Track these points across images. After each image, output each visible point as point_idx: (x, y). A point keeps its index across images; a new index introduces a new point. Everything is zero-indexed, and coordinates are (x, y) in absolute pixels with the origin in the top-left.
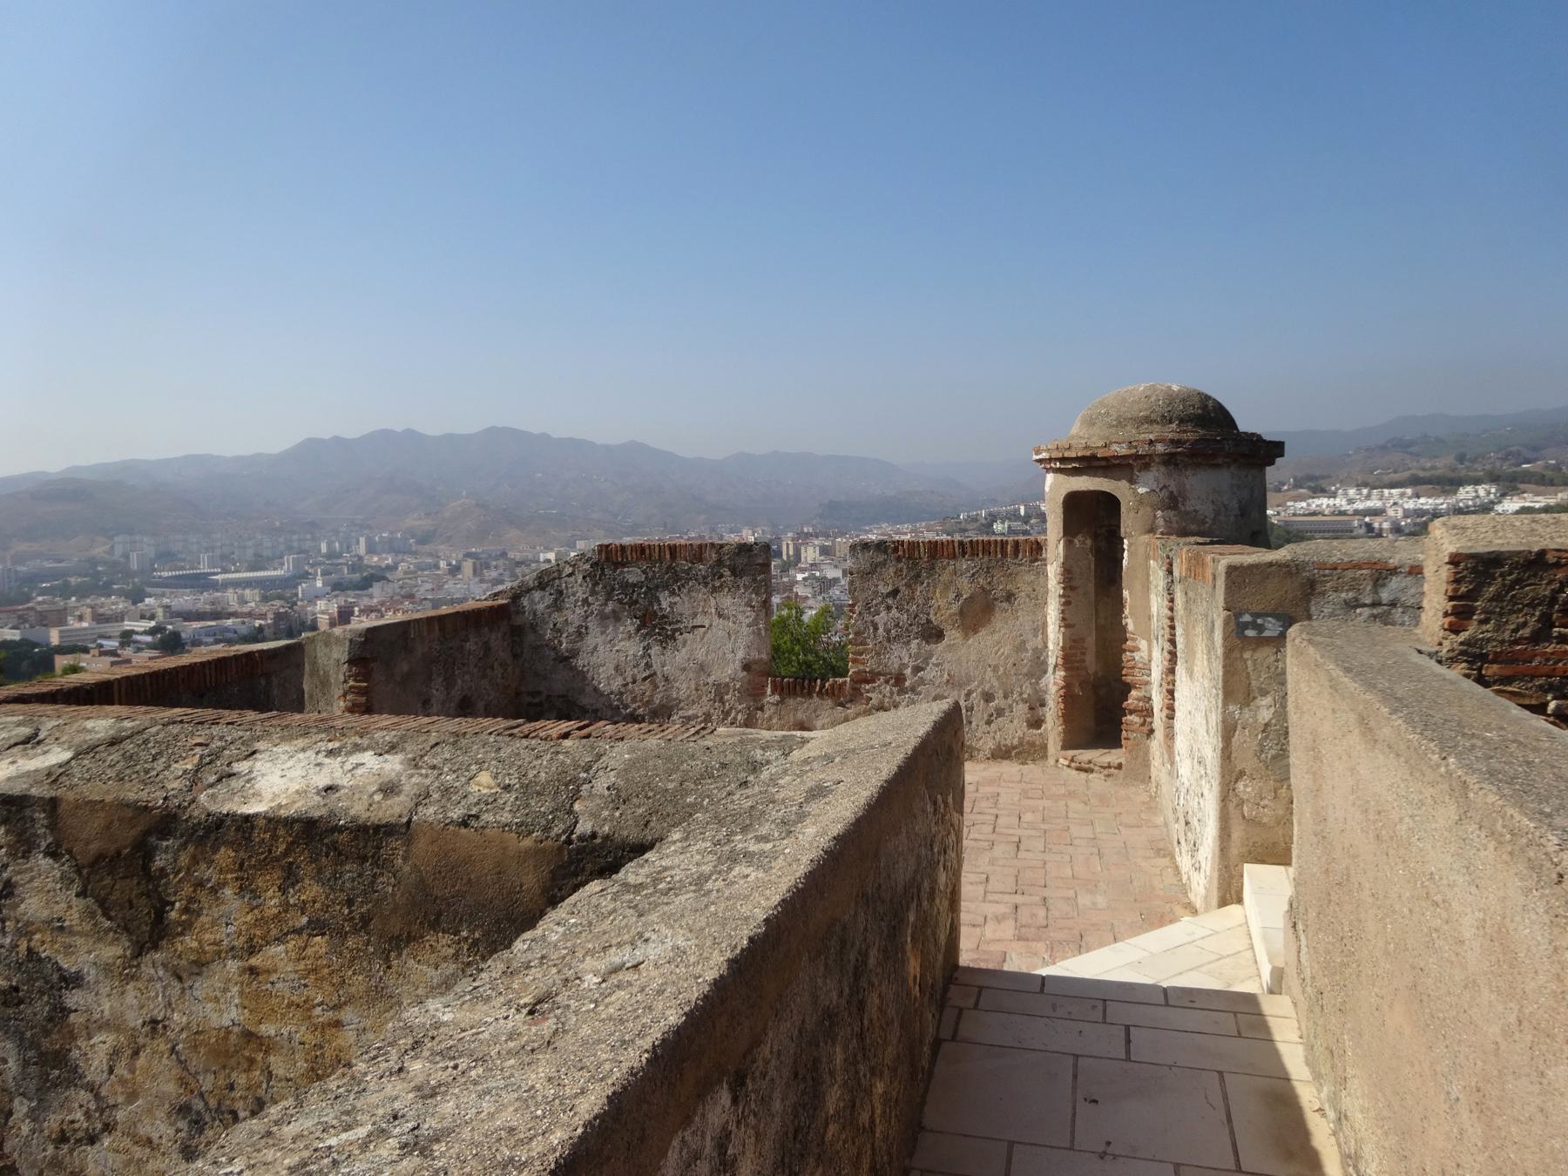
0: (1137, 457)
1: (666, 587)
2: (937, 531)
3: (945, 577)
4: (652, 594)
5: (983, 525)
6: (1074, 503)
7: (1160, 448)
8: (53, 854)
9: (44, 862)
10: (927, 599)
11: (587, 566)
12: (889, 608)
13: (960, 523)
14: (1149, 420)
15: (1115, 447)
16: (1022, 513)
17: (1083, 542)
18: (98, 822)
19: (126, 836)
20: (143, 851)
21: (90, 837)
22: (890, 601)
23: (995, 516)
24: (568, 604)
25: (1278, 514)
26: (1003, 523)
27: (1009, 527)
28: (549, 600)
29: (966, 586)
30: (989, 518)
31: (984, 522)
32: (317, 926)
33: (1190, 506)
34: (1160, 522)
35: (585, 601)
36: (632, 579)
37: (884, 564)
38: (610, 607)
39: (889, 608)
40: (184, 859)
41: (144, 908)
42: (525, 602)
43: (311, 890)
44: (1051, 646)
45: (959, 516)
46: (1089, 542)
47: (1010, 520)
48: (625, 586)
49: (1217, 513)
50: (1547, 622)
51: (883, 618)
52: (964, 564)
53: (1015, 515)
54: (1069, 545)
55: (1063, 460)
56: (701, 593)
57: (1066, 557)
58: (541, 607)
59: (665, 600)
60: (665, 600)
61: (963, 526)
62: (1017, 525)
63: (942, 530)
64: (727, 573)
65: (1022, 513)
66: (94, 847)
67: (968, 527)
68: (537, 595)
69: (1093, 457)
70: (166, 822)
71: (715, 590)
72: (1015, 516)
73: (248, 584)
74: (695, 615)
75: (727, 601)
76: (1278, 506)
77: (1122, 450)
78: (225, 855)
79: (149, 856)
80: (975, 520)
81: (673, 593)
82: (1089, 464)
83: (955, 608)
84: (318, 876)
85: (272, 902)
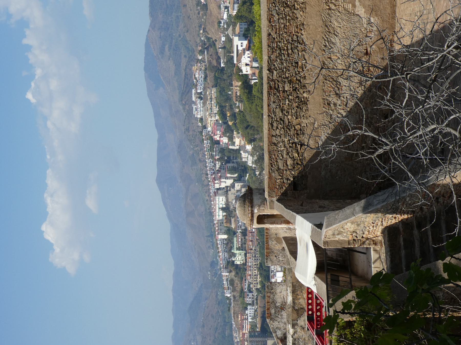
0: (251, 212)
1: (275, 304)
2: (242, 320)
3: (273, 247)
4: (276, 307)
5: (237, 273)
6: (259, 222)
7: (250, 209)
8: (297, 321)
9: (298, 322)
10: (277, 250)
11: (271, 321)
12: (279, 258)
13: (234, 297)
14: (244, 210)
15: (249, 216)
16: (225, 237)
17: (266, 221)
18: (294, 315)
19: (295, 312)
20: (296, 310)
21: (295, 316)
22: (277, 257)
23: (228, 262)
24: (279, 326)
25: (226, 7)
26: (234, 255)
27: (238, 249)
28: (278, 331)
29: (274, 242)
30: (230, 268)
31: (233, 273)
32: (302, 292)
33: (259, 204)
34: (262, 208)
35: (278, 322)
36: (274, 312)
37: (270, 259)
38: (279, 317)
39: (279, 258)
40: (297, 306)
41: (302, 310)
42: (279, 336)
43: (298, 292)
44: (285, 226)
45: (228, 298)
46: (266, 220)
47: (231, 248)
48: (275, 313)
49: (261, 199)
50: (274, 191)
51: (281, 259)
52: (270, 243)
53: (227, 244)
54: (266, 223)
55: (251, 225)
56: (276, 296)
57: (268, 224)
58: (280, 332)
59: (278, 304)
60: (278, 304)
61: (237, 294)
62: (237, 242)
63: (242, 315)
64: (272, 291)
65: (225, 237)
66: (296, 315)
67: (238, 289)
68: (277, 333)
69: (251, 220)
70: (293, 307)
71: (276, 294)
72: (229, 244)
73: (261, 78)
74: (281, 298)
75: (278, 291)
76: (219, 7)
77: (250, 215)
78: (296, 301)
79: (297, 310)
80: (232, 282)
81: (277, 303)
82: (252, 220)
83: (278, 245)
84: (297, 292)
85: (300, 296)
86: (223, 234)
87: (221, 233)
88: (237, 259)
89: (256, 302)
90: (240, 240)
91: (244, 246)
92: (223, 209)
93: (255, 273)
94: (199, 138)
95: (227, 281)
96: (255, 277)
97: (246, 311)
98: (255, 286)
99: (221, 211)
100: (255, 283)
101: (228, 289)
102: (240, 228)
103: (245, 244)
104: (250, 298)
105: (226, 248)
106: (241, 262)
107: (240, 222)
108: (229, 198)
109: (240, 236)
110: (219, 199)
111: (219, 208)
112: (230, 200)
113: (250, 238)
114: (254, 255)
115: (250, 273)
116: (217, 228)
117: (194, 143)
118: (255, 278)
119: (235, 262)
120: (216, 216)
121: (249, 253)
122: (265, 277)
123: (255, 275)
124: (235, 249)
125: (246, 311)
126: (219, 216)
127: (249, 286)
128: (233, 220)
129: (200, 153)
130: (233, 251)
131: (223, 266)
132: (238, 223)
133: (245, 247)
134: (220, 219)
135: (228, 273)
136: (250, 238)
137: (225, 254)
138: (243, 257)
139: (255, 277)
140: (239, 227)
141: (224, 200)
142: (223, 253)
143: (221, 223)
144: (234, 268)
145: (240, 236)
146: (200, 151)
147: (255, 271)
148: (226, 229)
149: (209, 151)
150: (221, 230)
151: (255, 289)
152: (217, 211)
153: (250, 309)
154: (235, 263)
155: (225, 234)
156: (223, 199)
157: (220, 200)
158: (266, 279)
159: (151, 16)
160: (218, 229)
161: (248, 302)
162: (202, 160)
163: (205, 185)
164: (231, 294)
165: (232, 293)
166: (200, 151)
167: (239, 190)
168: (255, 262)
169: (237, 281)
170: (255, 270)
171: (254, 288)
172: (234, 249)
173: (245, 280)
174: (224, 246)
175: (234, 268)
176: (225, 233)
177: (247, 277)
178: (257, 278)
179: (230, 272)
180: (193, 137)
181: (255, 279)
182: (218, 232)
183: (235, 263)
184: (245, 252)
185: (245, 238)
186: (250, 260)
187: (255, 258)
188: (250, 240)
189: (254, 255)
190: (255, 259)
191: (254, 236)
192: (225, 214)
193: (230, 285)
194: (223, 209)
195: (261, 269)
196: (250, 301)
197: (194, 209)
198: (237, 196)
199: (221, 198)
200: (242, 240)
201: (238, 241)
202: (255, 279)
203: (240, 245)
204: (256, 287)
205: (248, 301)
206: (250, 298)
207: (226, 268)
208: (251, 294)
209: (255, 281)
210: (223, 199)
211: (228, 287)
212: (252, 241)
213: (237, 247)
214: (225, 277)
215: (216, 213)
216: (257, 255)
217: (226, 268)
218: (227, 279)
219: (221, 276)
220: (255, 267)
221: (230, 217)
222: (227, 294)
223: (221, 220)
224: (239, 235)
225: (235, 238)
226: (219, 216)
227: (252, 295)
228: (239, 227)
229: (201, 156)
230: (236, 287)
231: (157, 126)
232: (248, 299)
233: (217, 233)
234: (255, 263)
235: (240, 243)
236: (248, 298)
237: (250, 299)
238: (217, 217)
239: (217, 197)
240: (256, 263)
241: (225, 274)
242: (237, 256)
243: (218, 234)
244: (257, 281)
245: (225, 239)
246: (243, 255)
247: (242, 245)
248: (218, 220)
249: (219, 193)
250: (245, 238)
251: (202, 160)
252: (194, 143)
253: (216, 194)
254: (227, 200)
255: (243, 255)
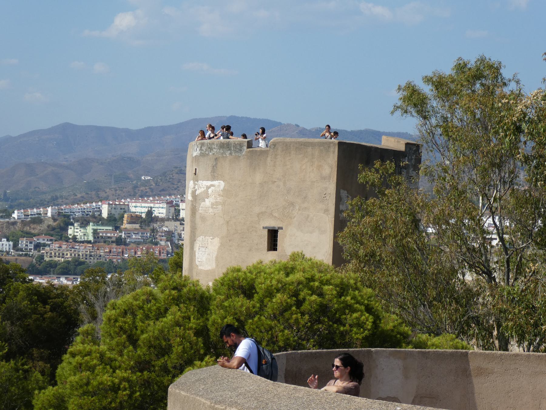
13: (14, 223)
16: (105, 215)
27: (95, 232)
31: (51, 223)
53: (94, 216)
65: (105, 215)
80: (38, 220)
86: (109, 211)
87: (110, 208)
88: (76, 230)
89: (22, 254)
90: (109, 235)
91: (102, 240)
92: (150, 213)
93: (67, 254)
94: (169, 187)
95: (38, 214)
96: (61, 254)
97: (5, 240)
98: (47, 253)
99: (146, 210)
100: (51, 253)
101: (25, 215)
102: (127, 236)
103: (105, 242)
104: (27, 245)
105: (87, 215)
106: (70, 235)
107: (136, 236)
108: (169, 222)
109: (116, 235)
110: (163, 208)
111: (151, 208)
112: (166, 223)
113: (115, 250)
114: (93, 254)
115: (64, 247)
116: (117, 203)
117: (161, 180)
118: (59, 254)
119: (72, 227)
120: (135, 202)
121: (93, 247)
122: (66, 268)
123: (63, 254)
124: (95, 228)
125: (5, 240)
126: (135, 207)
127: (45, 245)
128: (137, 226)
129: (147, 188)
130: (91, 224)
131: (62, 210)
132: (134, 233)
133: (99, 242)
134: (130, 208)
135: (52, 215)
136: (115, 250)
137: (79, 213)
138: (81, 238)
139: (61, 254)
140: (129, 235)
141: (161, 216)
142: (80, 211)
143: (125, 209)
144: (62, 225)
145: (116, 235)
146: (150, 188)
147: (69, 255)
148: (117, 216)
149: (96, 208)
150: (115, 208)
151: (43, 253)
152: (147, 205)
153: (10, 245)
154: (70, 227)
155: (108, 214)
156: (162, 213)
157: (160, 209)
158: (64, 269)
159: (318, 130)
160: (115, 204)
161: (20, 242)
162: (136, 191)
163: (99, 193)
164: (18, 219)
165: (20, 221)
166: (150, 188)
167: (181, 237)
168: (83, 255)
169: (44, 226)
170: (71, 255)
171: (44, 252)
172: (94, 225)
173: (51, 240)
174: (90, 212)
175: (62, 225)
176: (110, 214)
177: (57, 242)
178: (59, 257)
179: (55, 220)
180: (170, 178)
181: (57, 254)
182: (112, 204)
183: (70, 227)
184: (92, 242)
185: (113, 242)
186: (83, 247)
187: (88, 256)
188: (112, 250)
189: (93, 254)
190: (86, 255)
191: (118, 256)
192: (144, 216)
193: (31, 218)
194: (150, 213)
195: (77, 263)
196: (22, 245)
197: (38, 175)
198: (173, 234)
199: (164, 211)
200: (109, 237)
201: (107, 231)
202: (57, 254)
203: (101, 234)
204: (45, 254)
205: (22, 242)
206: (27, 245)
207: (59, 212)
208: (33, 247)
209: (55, 254)
210: (162, 213)
211: (28, 215)
212: (110, 252)
213: (98, 231)
214: (43, 211)
215: (140, 202)
216: (92, 258)
217: (59, 212)
218: (40, 214)
219: (45, 205)
220: (75, 255)
221: (141, 222)
222: (18, 213)
223: (129, 209)
224: (117, 234)
225: (111, 228)
226: (135, 207)
227: (31, 249)
228: (129, 235)
229: (141, 189)
230: (30, 227)
231: (149, 129)
232: (24, 242)
233: (111, 203)
234: (81, 255)
235: (104, 235)
236: (26, 242)
237: (24, 246)
238: (134, 204)
239: (165, 206)
240: (81, 257)
241: (50, 211)
242: (82, 230)
243: (109, 204)
244: (55, 257)
245: (101, 213)
246: (84, 238)
247: (102, 237)
248: (128, 205)
249: (171, 208)
250: (113, 242)
251: (136, 191)
252: (161, 180)
253: (170, 203)
254: (163, 220)
255: (84, 238)
